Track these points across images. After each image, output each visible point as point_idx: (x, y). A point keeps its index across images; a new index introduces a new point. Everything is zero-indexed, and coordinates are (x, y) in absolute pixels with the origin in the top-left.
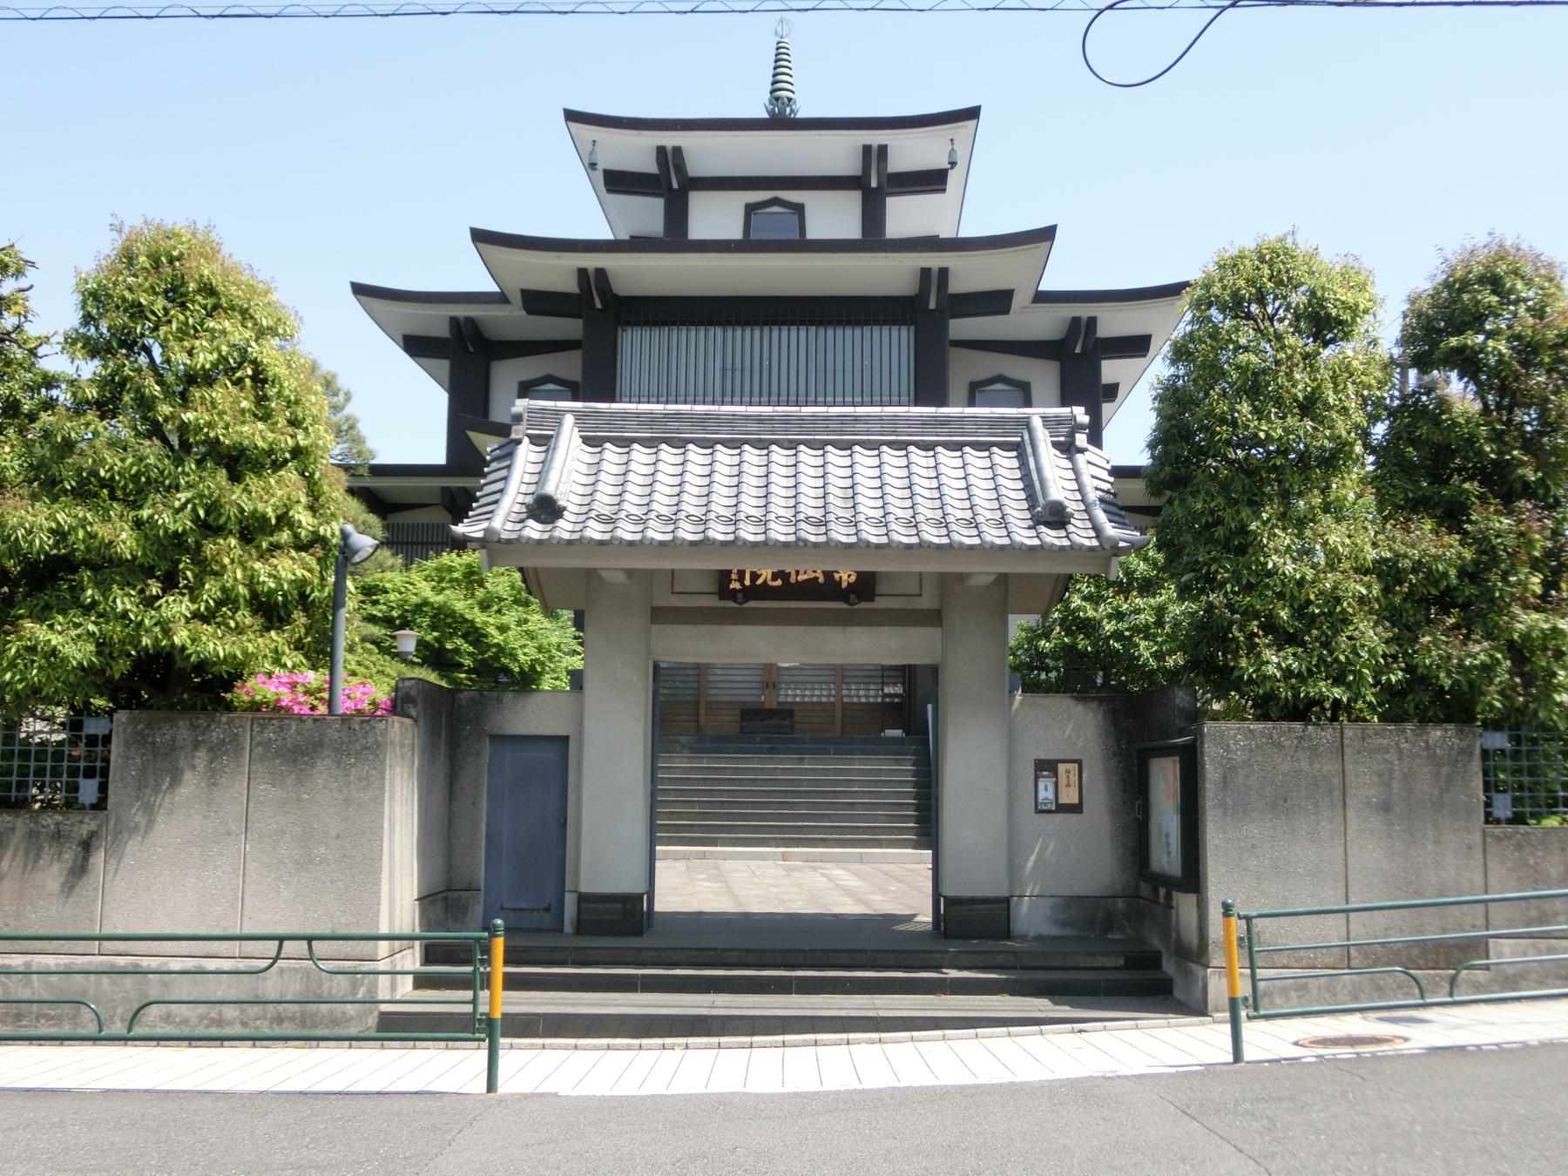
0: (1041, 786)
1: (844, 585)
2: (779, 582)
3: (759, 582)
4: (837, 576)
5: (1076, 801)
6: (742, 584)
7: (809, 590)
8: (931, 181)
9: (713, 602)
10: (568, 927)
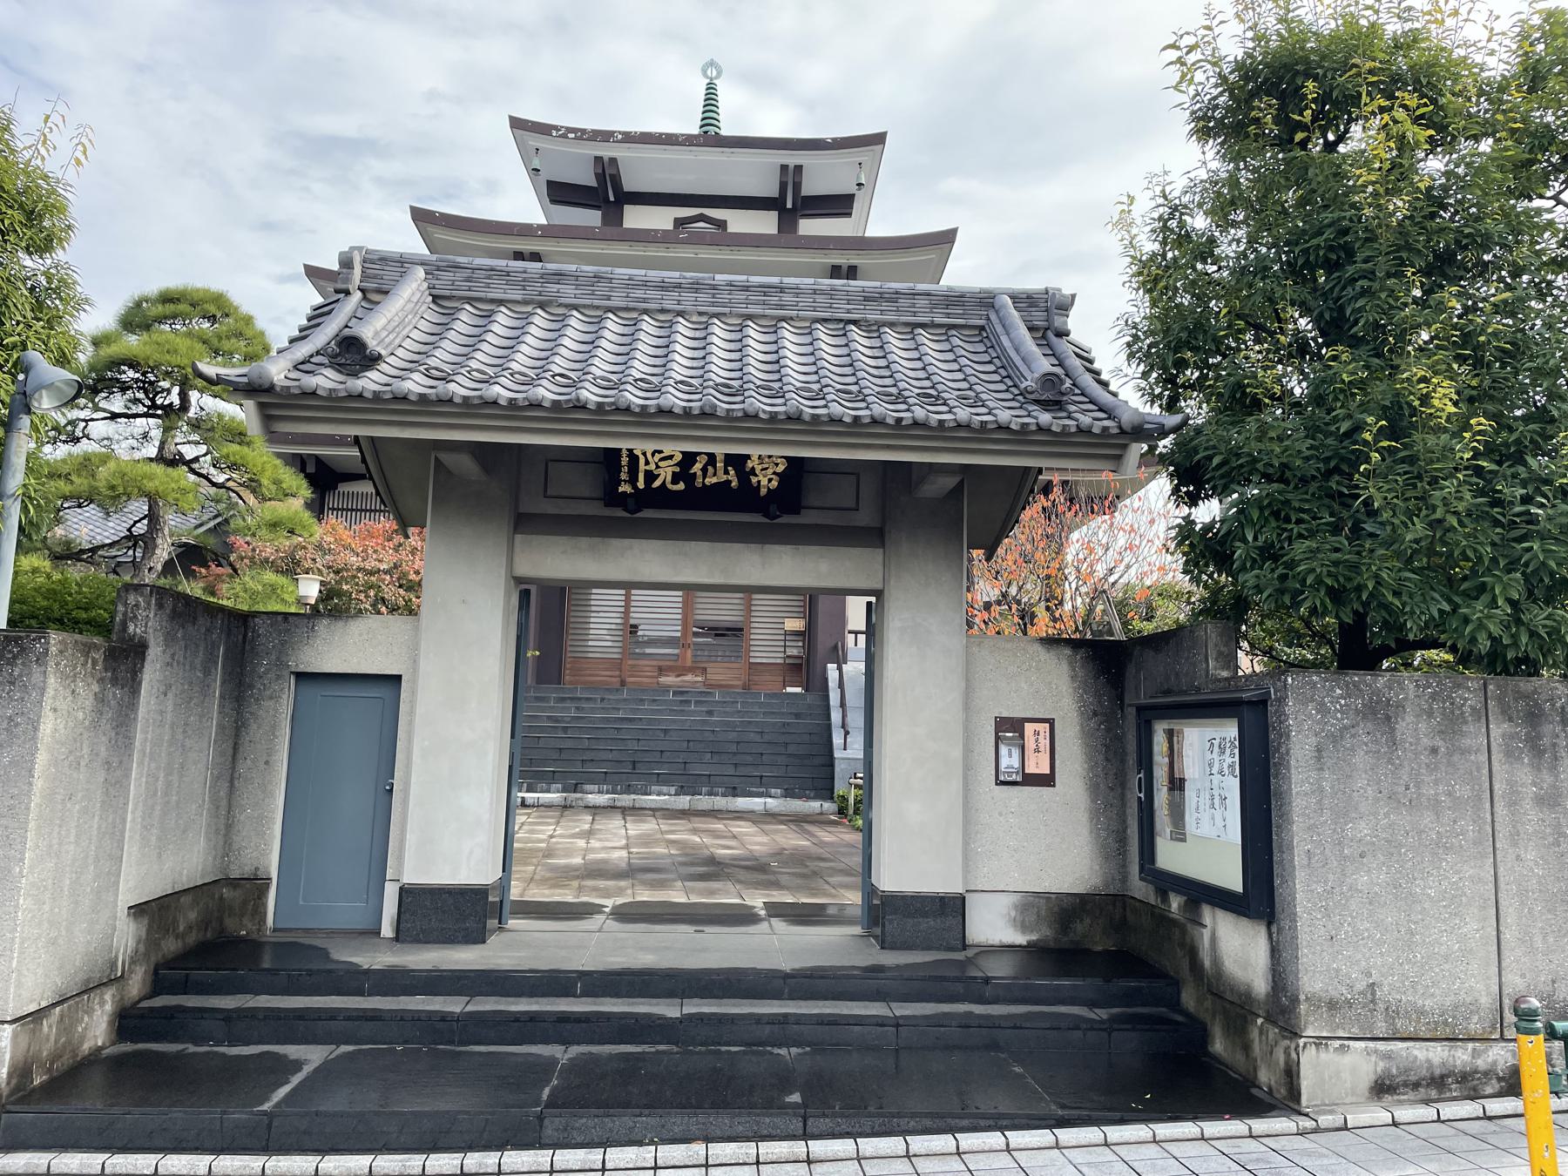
0: (1004, 750)
1: (763, 491)
2: (681, 486)
3: (657, 484)
4: (754, 480)
5: (1048, 772)
6: (635, 487)
7: (718, 497)
8: (839, 205)
9: (597, 509)
10: (387, 930)
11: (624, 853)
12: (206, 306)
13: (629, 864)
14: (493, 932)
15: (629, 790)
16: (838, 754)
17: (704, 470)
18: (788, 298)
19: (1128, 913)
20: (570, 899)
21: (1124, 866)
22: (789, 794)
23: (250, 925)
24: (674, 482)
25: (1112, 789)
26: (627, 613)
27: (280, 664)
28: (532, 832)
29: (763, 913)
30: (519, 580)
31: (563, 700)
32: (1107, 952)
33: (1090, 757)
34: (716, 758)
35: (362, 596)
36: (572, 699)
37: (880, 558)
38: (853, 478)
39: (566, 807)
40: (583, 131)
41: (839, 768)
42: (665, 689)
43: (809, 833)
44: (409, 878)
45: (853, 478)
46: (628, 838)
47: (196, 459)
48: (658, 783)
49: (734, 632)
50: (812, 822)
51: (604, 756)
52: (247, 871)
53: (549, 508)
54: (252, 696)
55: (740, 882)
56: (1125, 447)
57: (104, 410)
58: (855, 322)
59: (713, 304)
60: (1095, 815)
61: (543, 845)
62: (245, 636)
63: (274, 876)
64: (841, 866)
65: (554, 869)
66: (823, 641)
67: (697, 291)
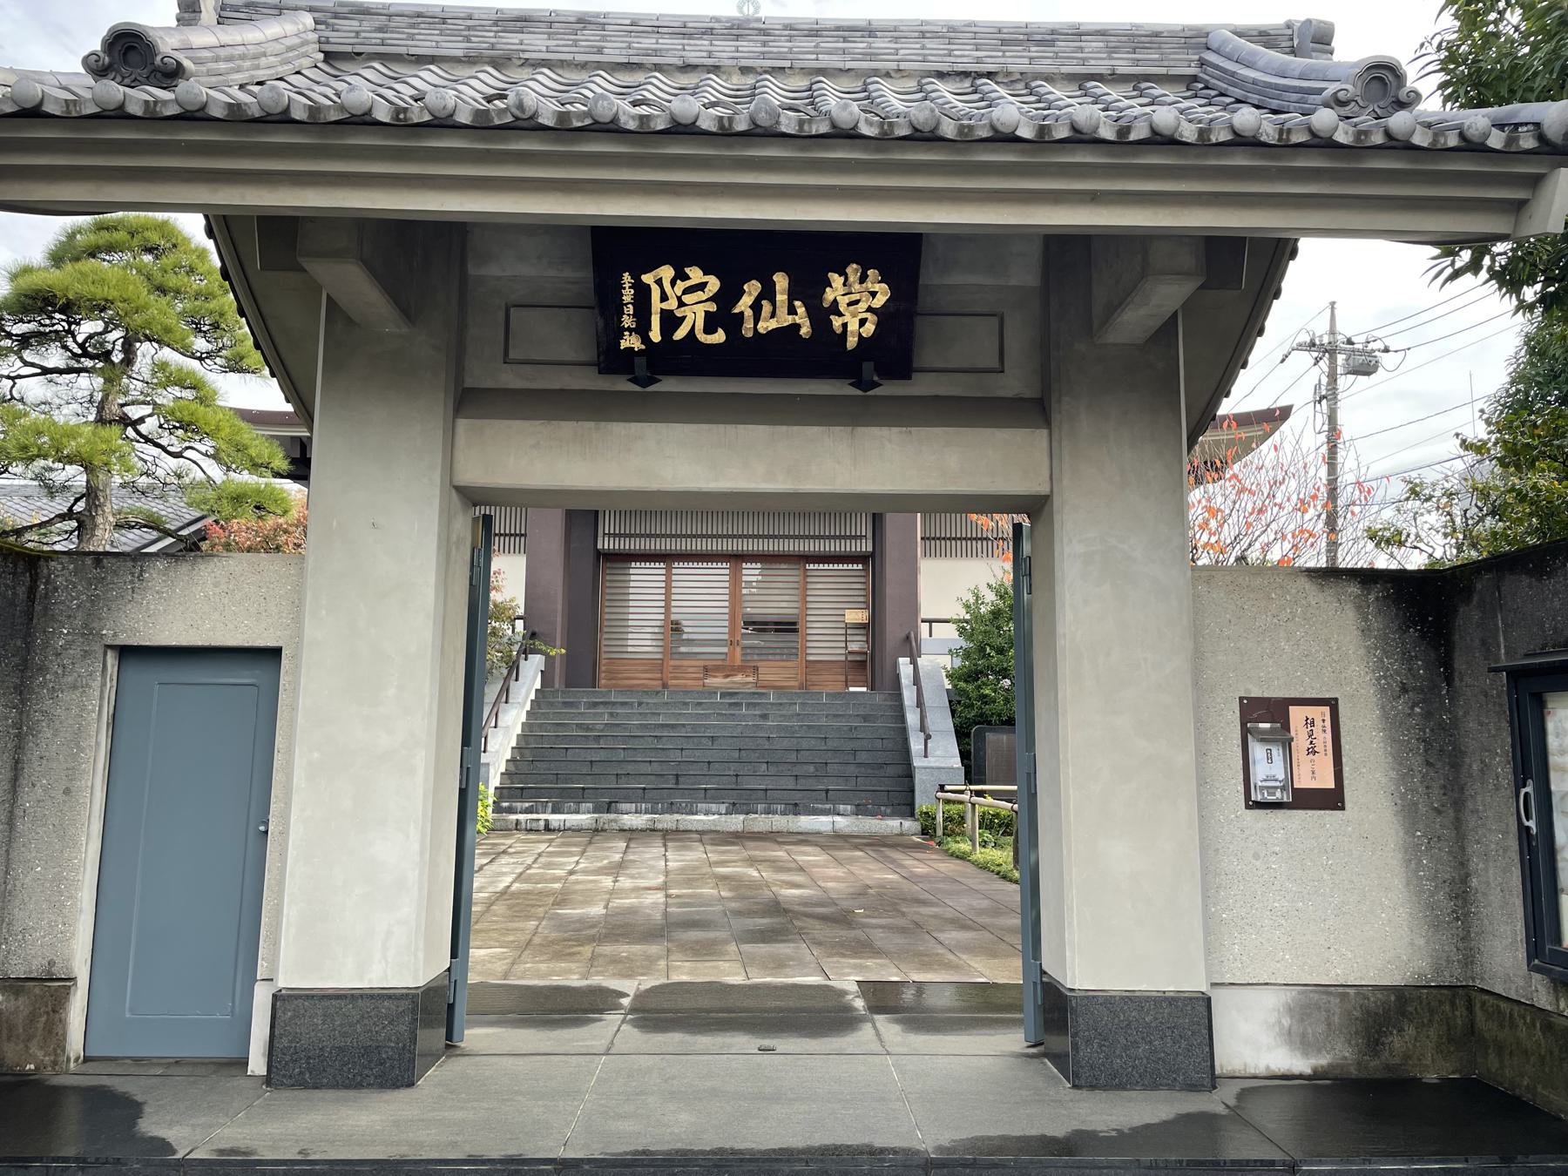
0: (1258, 751)
1: (852, 342)
2: (719, 337)
3: (680, 334)
4: (837, 322)
6: (646, 339)
10: (257, 1064)
11: (659, 897)
12: (148, 234)
13: (666, 914)
14: (433, 1058)
15: (671, 809)
16: (917, 762)
17: (756, 307)
18: (880, 44)
19: (1479, 1015)
20: (575, 981)
21: (1465, 938)
22: (860, 810)
23: (40, 1054)
24: (709, 329)
25: (1439, 812)
26: (667, 607)
27: (89, 632)
28: (549, 866)
29: (859, 1004)
30: (471, 496)
31: (595, 705)
32: (1446, 1082)
33: (1398, 760)
34: (773, 770)
37: (1045, 444)
38: (994, 321)
39: (597, 831)
41: (919, 777)
43: (893, 861)
44: (288, 979)
45: (994, 321)
46: (667, 873)
47: (142, 420)
48: (705, 800)
49: (787, 627)
50: (894, 846)
51: (647, 769)
52: (36, 967)
53: (510, 379)
54: (43, 685)
55: (819, 944)
56: (1535, 182)
57: (33, 365)
58: (990, 75)
59: (764, 56)
60: (1412, 854)
61: (557, 886)
62: (32, 590)
63: (81, 970)
64: (949, 913)
65: (562, 924)
66: (893, 632)
67: (738, 37)
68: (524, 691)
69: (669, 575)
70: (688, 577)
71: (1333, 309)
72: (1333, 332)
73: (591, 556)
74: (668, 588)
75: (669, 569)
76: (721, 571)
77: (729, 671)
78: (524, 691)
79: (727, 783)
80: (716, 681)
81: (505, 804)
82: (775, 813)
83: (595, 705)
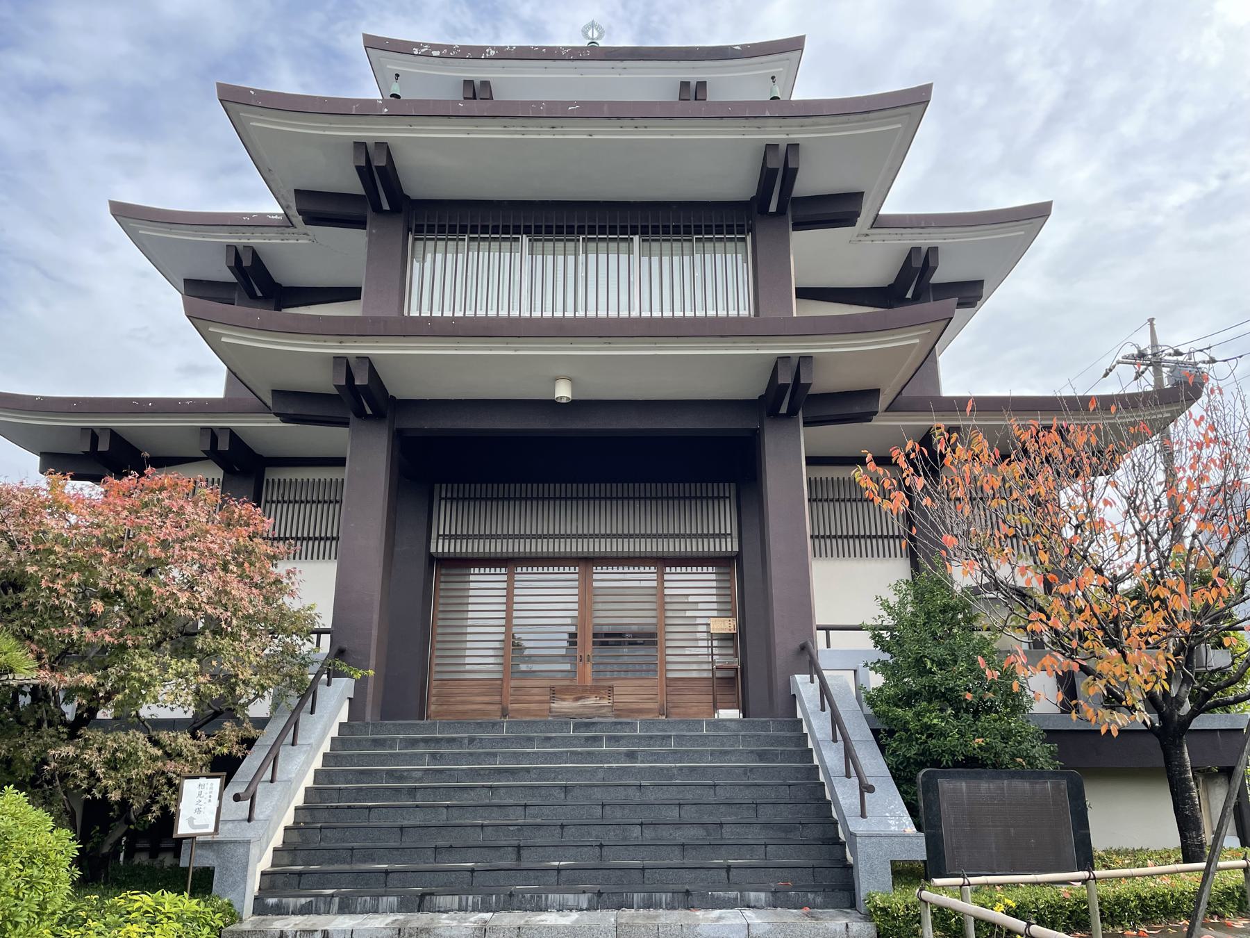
15: (510, 903)
31: (413, 743)
35: (59, 584)
36: (426, 741)
40: (450, 48)
42: (563, 720)
68: (319, 727)
69: (511, 581)
70: (530, 583)
71: (1152, 325)
72: (1154, 344)
73: (422, 562)
74: (510, 596)
75: (511, 575)
76: (569, 577)
77: (580, 693)
78: (319, 727)
79: (589, 858)
80: (565, 705)
81: (272, 901)
82: (657, 906)
83: (413, 743)
